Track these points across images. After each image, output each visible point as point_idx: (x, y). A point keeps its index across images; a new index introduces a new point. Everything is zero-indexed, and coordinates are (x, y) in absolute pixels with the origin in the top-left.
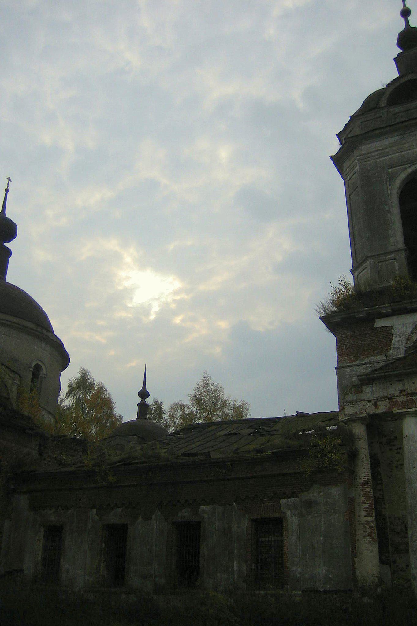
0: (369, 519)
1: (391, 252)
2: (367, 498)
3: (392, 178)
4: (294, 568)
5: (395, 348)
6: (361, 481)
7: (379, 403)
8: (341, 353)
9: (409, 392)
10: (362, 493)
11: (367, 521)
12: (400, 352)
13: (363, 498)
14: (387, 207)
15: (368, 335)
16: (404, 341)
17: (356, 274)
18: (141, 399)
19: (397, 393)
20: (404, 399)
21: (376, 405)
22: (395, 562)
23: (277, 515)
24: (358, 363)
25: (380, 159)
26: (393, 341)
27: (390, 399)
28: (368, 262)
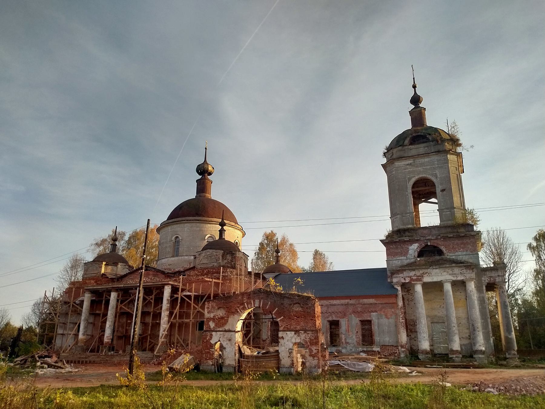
0: (403, 321)
2: (402, 313)
3: (410, 179)
4: (377, 338)
5: (410, 254)
6: (400, 307)
7: (406, 279)
8: (388, 255)
13: (400, 313)
16: (414, 252)
17: (392, 219)
18: (221, 227)
19: (413, 275)
20: (416, 278)
21: (405, 279)
22: (410, 335)
23: (369, 319)
24: (395, 259)
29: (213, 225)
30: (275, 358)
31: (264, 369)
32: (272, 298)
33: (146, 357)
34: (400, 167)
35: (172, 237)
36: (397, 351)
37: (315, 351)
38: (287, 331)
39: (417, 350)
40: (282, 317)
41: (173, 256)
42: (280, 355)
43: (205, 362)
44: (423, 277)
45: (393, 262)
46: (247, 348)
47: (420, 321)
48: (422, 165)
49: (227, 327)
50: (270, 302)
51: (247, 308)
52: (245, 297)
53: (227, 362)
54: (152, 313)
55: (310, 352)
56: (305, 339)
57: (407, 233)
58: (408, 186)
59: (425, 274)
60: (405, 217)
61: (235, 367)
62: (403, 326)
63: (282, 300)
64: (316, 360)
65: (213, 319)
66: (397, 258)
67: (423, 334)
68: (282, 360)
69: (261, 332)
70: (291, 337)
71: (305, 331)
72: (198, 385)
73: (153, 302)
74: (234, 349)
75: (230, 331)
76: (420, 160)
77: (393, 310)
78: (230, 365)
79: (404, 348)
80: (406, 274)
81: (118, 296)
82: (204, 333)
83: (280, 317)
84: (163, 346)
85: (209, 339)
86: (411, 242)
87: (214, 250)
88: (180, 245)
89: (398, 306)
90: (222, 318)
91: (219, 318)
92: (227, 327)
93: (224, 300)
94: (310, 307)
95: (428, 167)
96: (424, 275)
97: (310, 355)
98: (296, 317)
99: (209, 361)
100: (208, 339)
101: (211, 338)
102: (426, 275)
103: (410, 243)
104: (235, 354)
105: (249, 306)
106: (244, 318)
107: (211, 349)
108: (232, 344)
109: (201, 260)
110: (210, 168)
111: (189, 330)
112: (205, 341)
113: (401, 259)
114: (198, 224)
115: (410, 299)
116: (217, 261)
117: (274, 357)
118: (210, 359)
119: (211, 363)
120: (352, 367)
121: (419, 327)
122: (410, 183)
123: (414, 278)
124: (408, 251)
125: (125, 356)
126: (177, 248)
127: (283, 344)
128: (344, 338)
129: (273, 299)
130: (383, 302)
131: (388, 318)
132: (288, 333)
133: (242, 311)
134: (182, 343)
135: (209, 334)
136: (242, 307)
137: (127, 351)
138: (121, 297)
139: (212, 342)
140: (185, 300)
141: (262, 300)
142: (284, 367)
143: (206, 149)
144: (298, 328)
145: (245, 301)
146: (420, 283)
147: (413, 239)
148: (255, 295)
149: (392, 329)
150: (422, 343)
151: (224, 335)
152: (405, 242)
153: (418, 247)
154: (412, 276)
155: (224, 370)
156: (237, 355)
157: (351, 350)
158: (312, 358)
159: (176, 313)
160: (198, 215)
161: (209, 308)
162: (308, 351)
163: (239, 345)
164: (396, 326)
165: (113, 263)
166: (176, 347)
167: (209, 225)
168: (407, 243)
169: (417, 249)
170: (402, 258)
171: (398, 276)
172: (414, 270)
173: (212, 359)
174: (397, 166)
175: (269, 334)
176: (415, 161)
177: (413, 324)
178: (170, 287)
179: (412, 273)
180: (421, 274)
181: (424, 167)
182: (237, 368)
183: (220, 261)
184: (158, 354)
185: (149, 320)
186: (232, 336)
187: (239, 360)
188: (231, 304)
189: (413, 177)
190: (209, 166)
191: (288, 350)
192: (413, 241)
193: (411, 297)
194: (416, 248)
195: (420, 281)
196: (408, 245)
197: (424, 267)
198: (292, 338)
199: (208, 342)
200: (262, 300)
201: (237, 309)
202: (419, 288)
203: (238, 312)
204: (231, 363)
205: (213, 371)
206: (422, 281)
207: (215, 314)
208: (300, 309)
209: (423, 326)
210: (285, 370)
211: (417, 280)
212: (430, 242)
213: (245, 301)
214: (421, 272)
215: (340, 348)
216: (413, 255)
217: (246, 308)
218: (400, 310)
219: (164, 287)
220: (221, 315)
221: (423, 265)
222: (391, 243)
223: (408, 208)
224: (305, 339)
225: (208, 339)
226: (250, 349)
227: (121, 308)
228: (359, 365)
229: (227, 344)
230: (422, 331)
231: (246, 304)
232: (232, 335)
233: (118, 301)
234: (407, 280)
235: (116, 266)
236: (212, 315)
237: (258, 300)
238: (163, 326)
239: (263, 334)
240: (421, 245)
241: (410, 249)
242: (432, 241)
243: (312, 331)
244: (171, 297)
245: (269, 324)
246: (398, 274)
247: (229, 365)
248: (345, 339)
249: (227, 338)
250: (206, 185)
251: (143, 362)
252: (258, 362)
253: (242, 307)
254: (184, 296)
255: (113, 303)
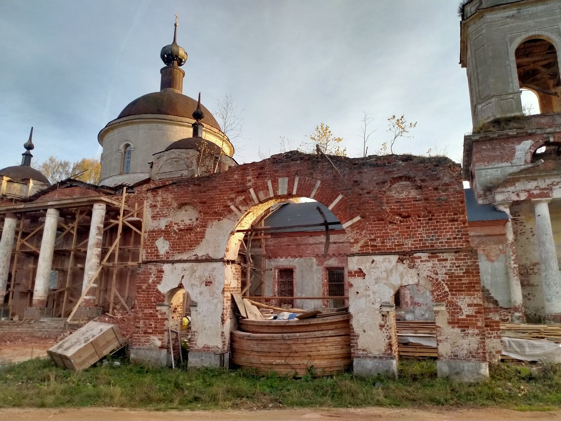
0: (516, 266)
1: (511, 94)
3: (512, 40)
6: (510, 242)
7: (520, 194)
9: (541, 187)
10: (511, 250)
11: (515, 267)
12: (521, 161)
13: (511, 253)
14: (507, 62)
15: (497, 149)
16: (524, 154)
19: (533, 188)
21: (518, 195)
24: (490, 167)
25: (502, 27)
26: (516, 154)
27: (528, 191)
28: (493, 100)
29: (185, 128)
30: (336, 328)
31: (305, 362)
32: (325, 170)
33: (56, 328)
34: (495, 21)
35: (119, 146)
36: (509, 317)
37: (467, 311)
38: (375, 254)
39: (533, 315)
40: (358, 218)
41: (121, 174)
42: (354, 323)
43: (143, 340)
44: (551, 190)
45: (486, 172)
46: (253, 304)
47: (549, 264)
48: (533, 16)
49: (200, 251)
50: (319, 182)
51: (256, 201)
52: (251, 173)
53: (201, 341)
54: (72, 253)
55: (452, 314)
56: (434, 276)
57: (512, 124)
58: (510, 51)
59: (555, 185)
60: (505, 101)
61: (222, 355)
62: (517, 275)
63: (356, 172)
64: (473, 335)
65: (166, 233)
66: (494, 165)
67: (554, 287)
68: (361, 337)
69: (263, 286)
70: (386, 271)
71: (434, 253)
72: (400, 175)
73: (74, 233)
74: (220, 306)
75: (209, 260)
76: (528, 9)
77: (501, 247)
78: (208, 348)
79: (519, 312)
80: (519, 186)
81: (18, 226)
82: (143, 266)
83: (352, 218)
84: (88, 309)
85: (154, 282)
86: (520, 137)
87: (183, 150)
88: (132, 157)
89: (506, 240)
90: (189, 229)
91: (180, 230)
92: (200, 251)
93: (194, 185)
94: (446, 185)
95: (544, 19)
96: (554, 187)
97: (453, 323)
98: (400, 215)
99: (152, 337)
100: (151, 281)
101: (159, 278)
102: (558, 187)
103: (517, 140)
104: (223, 321)
105: (262, 196)
106: (247, 227)
107: (158, 308)
108: (214, 293)
109: (161, 167)
110: (181, 53)
111: (73, 238)
112: (144, 287)
113: (502, 167)
114: (160, 125)
115: (519, 232)
116: (188, 167)
117: (333, 326)
118: (155, 332)
119: (159, 343)
120: (516, 352)
121: (546, 276)
122: (512, 46)
123: (535, 192)
124: (514, 153)
125: (21, 324)
126: (128, 161)
127: (361, 291)
128: (409, 296)
129: (330, 171)
130: (482, 234)
131: (492, 261)
132: (377, 258)
133: (243, 208)
134: (123, 302)
135: (153, 268)
136: (241, 198)
137: (26, 317)
138: (23, 227)
139: (164, 288)
140: (131, 229)
141: (297, 179)
142: (366, 357)
143: (175, 25)
144: (409, 244)
145: (249, 184)
146: (546, 201)
147: (522, 133)
148: (279, 167)
149: (499, 278)
150: (553, 303)
151: (194, 271)
152: (508, 138)
153: (533, 145)
154: (531, 190)
155: (193, 361)
156: (228, 322)
157: (423, 315)
158: (457, 330)
159: (114, 250)
160: (159, 112)
161: (155, 206)
162: (443, 308)
163: (232, 296)
164: (507, 274)
165: (23, 180)
166: (113, 310)
167: (177, 127)
168: (511, 140)
169: (530, 148)
170: (504, 164)
171: (504, 189)
172: (535, 179)
173: (162, 333)
174: (488, 20)
175: (276, 290)
176: (521, 11)
177: (525, 273)
178: (104, 206)
179: (531, 185)
180: (548, 186)
181: (537, 20)
182: (227, 356)
183: (194, 167)
184: (76, 322)
185: (69, 264)
186: (214, 273)
187: (232, 334)
188: (211, 194)
189: (519, 36)
190: (180, 48)
191: (377, 306)
192: (523, 136)
193: (521, 228)
194: (528, 147)
195: (546, 197)
196: (513, 143)
197: (556, 172)
198: (389, 272)
199: (152, 289)
200: (297, 179)
201: (229, 204)
202: (543, 209)
203: (230, 211)
204: (211, 344)
205: (164, 363)
206: (550, 197)
207: (170, 219)
208: (413, 193)
209: (554, 273)
210: (369, 364)
211: (542, 195)
212: (554, 137)
213: (249, 184)
214: (548, 182)
215: (403, 312)
216: (523, 160)
217: (251, 200)
218: (511, 247)
219: (92, 206)
220: (188, 222)
221: (553, 170)
222: (483, 141)
223: (511, 85)
224: (434, 276)
225: (151, 281)
226: (258, 307)
227: (23, 246)
228: (533, 347)
229: (201, 293)
230: (552, 283)
231: (252, 191)
232: (214, 268)
233: (17, 233)
234: (523, 197)
235: (26, 184)
236: (162, 224)
237: (287, 179)
238: (90, 273)
239: (266, 290)
240: (537, 142)
241: (517, 149)
242: (557, 136)
243: (456, 252)
244: (106, 225)
245: (277, 274)
246: (506, 187)
247: (207, 349)
248: (411, 297)
249: (200, 277)
250: (175, 76)
251: (47, 337)
252: (289, 342)
253: (241, 198)
254: (128, 222)
255: (7, 236)
